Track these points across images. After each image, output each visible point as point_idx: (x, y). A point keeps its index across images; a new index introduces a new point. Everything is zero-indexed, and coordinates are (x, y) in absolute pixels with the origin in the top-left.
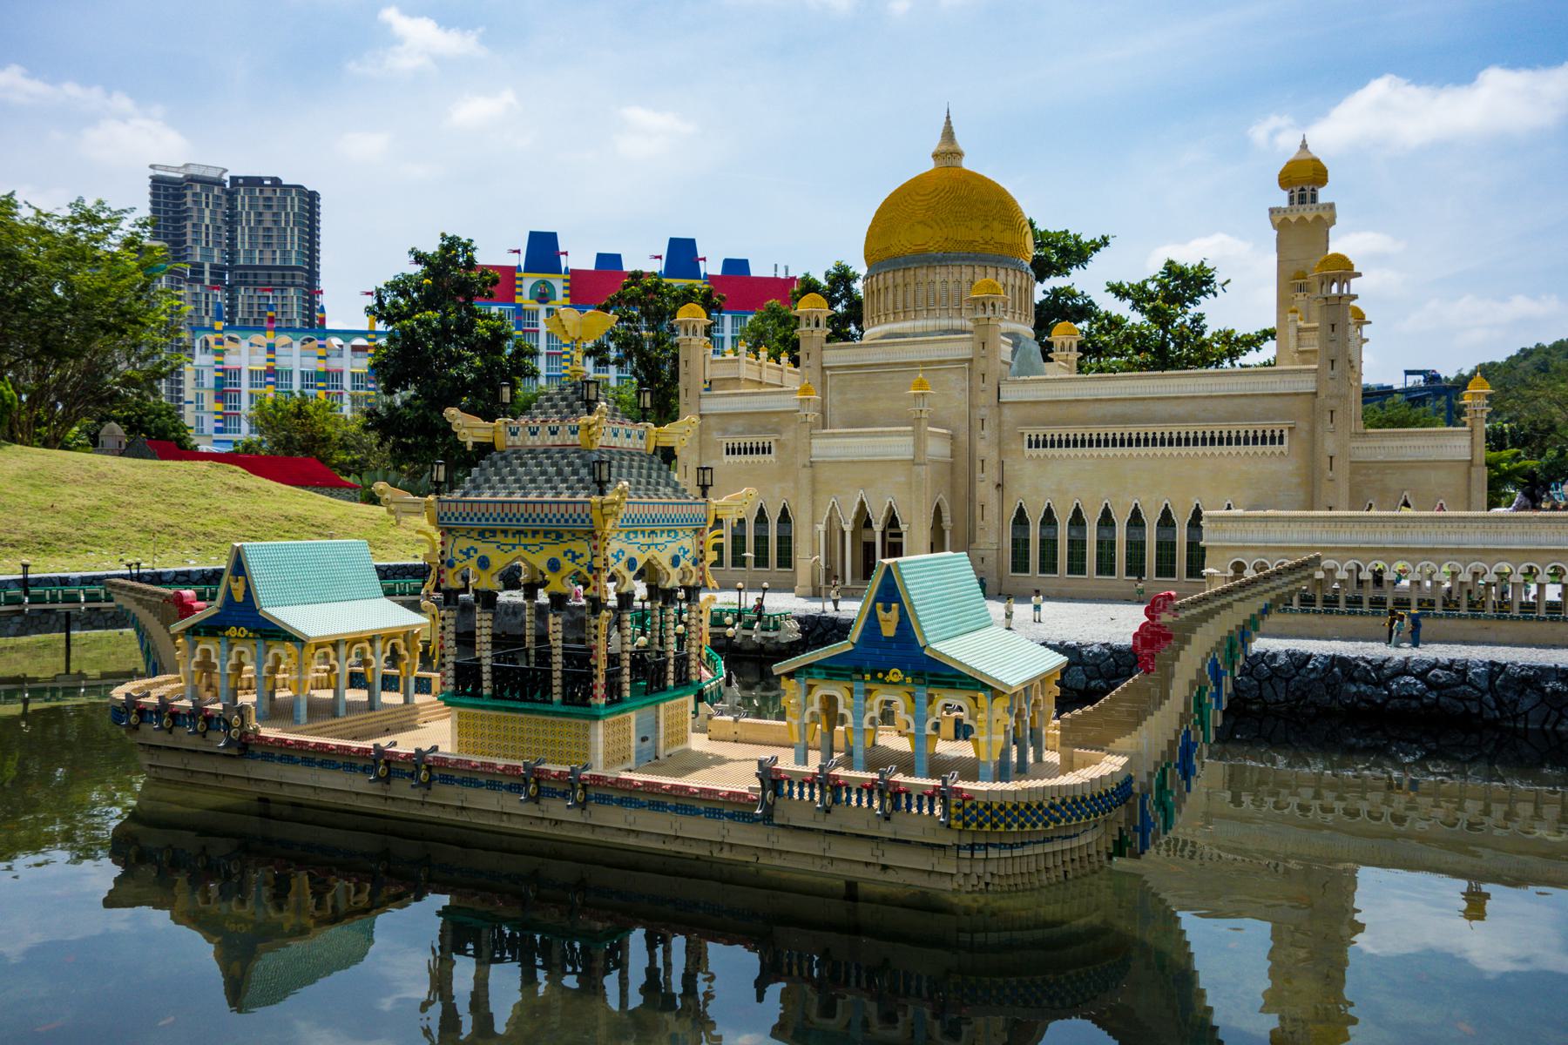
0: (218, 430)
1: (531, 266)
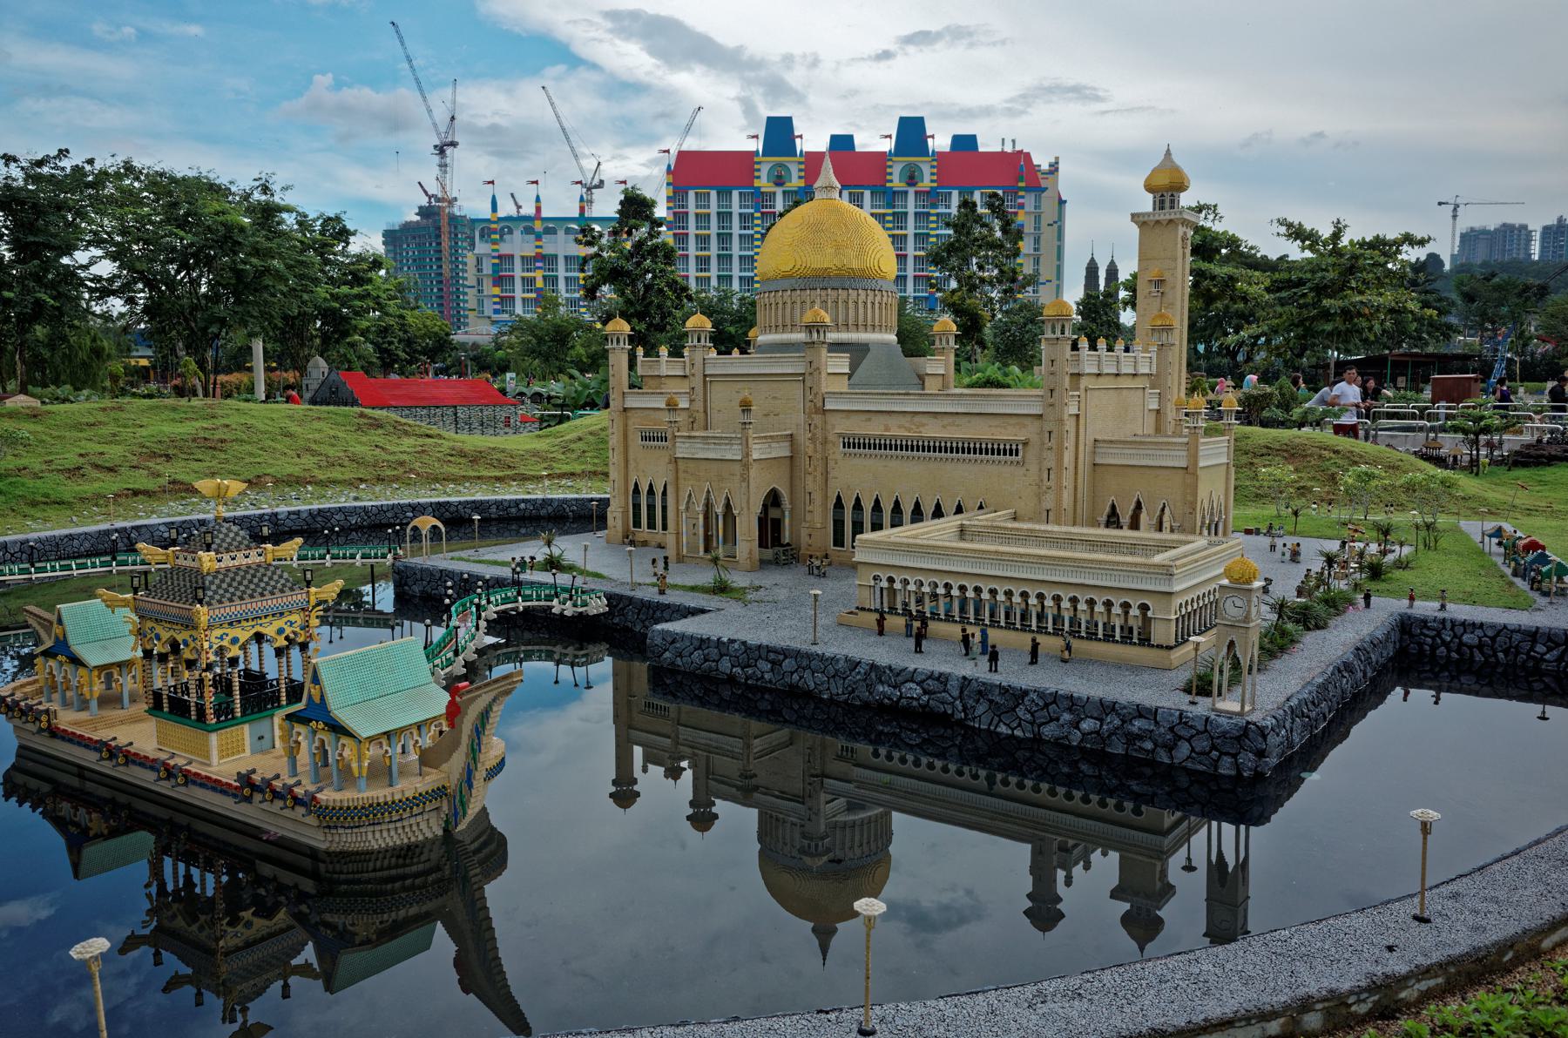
0: (496, 311)
1: (768, 151)
